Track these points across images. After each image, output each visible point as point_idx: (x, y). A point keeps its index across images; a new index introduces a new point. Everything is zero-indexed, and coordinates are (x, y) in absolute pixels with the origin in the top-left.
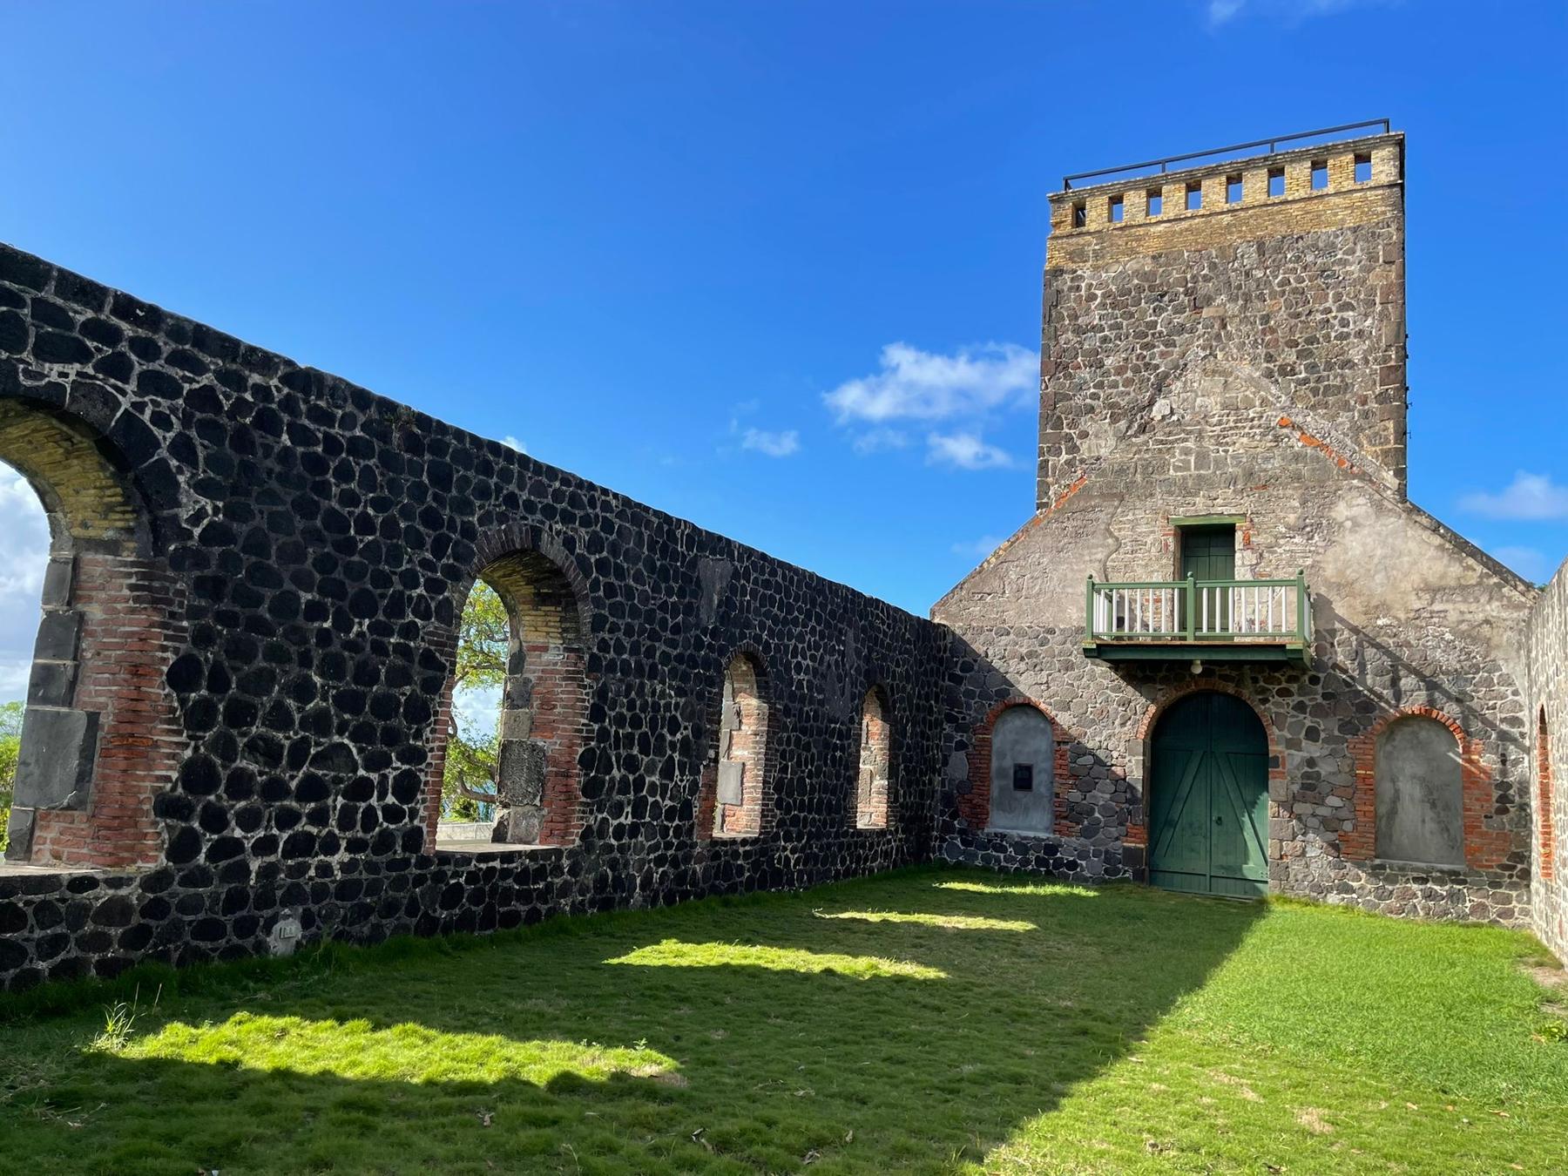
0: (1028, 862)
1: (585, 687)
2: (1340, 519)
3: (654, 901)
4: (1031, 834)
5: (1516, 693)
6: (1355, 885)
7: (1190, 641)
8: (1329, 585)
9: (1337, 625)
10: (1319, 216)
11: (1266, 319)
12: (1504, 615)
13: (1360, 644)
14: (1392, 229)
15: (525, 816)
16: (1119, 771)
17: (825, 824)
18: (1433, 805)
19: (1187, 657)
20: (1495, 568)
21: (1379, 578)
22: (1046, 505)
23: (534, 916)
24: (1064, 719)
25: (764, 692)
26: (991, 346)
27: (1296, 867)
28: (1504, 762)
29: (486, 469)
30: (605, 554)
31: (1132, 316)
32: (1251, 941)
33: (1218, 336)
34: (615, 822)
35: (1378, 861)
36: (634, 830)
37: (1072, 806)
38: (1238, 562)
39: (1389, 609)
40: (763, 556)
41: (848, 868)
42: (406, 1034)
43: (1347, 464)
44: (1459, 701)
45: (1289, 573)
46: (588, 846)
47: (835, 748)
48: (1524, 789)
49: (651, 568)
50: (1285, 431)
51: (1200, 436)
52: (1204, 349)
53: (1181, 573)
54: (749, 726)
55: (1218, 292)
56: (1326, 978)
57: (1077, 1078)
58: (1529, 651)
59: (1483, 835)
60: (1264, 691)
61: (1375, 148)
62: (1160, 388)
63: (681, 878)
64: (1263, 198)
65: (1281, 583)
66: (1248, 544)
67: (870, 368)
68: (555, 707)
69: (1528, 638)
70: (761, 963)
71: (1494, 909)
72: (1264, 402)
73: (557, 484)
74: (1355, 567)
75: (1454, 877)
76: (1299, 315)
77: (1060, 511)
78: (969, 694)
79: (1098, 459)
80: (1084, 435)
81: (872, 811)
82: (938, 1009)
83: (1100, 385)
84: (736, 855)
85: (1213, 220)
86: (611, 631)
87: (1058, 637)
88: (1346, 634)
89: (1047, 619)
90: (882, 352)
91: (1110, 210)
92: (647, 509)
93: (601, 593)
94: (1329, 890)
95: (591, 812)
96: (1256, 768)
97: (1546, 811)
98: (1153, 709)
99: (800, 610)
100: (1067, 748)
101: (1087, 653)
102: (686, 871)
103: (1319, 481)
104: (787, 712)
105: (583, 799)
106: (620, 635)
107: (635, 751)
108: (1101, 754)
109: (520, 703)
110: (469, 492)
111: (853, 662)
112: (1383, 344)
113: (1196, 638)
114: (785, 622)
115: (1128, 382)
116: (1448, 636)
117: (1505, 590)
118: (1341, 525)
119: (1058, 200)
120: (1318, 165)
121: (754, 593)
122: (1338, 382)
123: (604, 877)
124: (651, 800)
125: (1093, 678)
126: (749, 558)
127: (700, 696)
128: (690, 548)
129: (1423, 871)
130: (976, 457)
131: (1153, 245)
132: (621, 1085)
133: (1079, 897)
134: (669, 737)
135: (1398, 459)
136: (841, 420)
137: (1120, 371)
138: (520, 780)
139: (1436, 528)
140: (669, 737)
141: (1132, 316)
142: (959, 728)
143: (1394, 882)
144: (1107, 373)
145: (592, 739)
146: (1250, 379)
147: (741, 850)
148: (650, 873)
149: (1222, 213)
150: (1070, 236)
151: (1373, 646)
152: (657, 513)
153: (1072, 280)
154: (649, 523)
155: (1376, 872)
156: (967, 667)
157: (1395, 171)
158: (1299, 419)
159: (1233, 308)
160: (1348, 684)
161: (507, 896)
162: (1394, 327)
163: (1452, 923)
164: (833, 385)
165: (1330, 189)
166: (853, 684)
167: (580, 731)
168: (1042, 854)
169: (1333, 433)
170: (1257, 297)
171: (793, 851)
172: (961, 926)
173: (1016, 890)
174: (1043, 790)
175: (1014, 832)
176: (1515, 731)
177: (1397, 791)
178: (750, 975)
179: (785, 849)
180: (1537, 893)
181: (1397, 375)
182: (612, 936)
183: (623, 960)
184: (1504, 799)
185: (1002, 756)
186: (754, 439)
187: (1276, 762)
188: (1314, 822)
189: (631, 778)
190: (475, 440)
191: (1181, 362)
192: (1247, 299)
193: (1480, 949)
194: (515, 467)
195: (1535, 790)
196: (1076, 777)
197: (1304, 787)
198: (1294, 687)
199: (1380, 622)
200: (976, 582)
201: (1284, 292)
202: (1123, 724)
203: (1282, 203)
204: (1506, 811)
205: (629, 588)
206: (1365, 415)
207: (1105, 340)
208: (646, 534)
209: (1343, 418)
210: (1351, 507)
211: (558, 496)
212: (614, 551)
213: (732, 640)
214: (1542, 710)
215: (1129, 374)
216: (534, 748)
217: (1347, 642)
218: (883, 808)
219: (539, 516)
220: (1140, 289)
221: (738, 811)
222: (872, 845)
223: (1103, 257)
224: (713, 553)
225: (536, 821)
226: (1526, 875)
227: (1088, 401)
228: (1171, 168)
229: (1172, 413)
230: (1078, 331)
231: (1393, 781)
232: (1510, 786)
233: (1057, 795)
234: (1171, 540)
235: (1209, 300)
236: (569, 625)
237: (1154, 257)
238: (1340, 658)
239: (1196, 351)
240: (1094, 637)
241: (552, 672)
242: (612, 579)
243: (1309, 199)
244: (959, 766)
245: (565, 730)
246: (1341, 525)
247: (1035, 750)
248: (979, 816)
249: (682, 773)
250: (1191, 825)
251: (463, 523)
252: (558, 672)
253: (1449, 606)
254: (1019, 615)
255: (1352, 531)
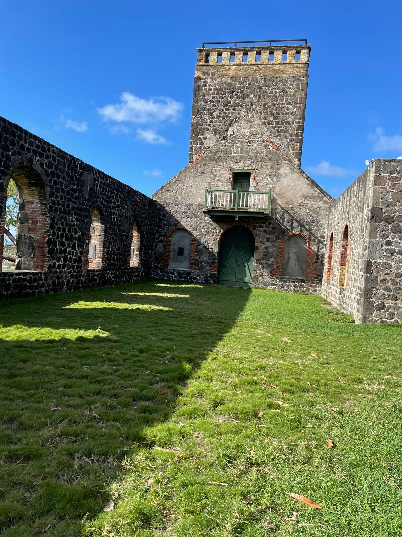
0: (181, 278)
1: (48, 217)
2: (281, 173)
3: (70, 290)
4: (183, 269)
5: (324, 229)
6: (276, 283)
7: (236, 210)
8: (277, 194)
9: (278, 207)
10: (283, 71)
11: (265, 105)
12: (323, 205)
13: (284, 213)
14: (305, 79)
15: (28, 261)
16: (210, 250)
17: (121, 265)
18: (298, 261)
19: (235, 215)
20: (322, 191)
21: (291, 192)
22: (192, 162)
23: (34, 294)
24: (195, 233)
25: (103, 221)
26: (162, 98)
27: (260, 279)
28: (318, 249)
29: (13, 134)
30: (53, 169)
31: (223, 98)
32: (251, 298)
33: (250, 109)
34: (58, 263)
35: (282, 277)
36: (64, 266)
37: (196, 261)
38: (251, 185)
39: (293, 202)
40: (103, 173)
41: (127, 279)
42: (18, 328)
43: (285, 156)
44: (308, 231)
45: (266, 190)
46: (50, 271)
47: (124, 241)
48: (323, 256)
49: (68, 175)
50: (268, 143)
51: (242, 143)
52: (245, 113)
53: (234, 188)
54: (98, 233)
55: (251, 93)
56: (274, 308)
57: (225, 333)
58: (329, 217)
59: (311, 269)
60: (255, 226)
61: (302, 49)
62: (231, 125)
63: (78, 282)
64: (267, 61)
65: (263, 193)
66: (254, 179)
67: (116, 100)
68: (37, 223)
69: (329, 213)
70: (115, 307)
71: (312, 289)
72: (262, 133)
73: (37, 142)
74: (284, 189)
75: (302, 281)
76: (275, 104)
77: (197, 164)
78: (165, 225)
79: (209, 147)
80: (205, 138)
81: (134, 262)
82: (177, 318)
83: (211, 122)
84: (94, 275)
85: (251, 67)
86: (56, 198)
87: (194, 207)
88: (280, 209)
89: (191, 201)
90: (122, 95)
91: (218, 57)
92: (67, 154)
93: (52, 184)
94: (269, 285)
95: (51, 260)
96: (251, 250)
97: (330, 262)
98: (222, 231)
99: (114, 193)
100: (195, 243)
101: (205, 212)
102: (80, 280)
103: (276, 160)
104: (110, 228)
105: (48, 255)
106: (59, 199)
107: (64, 240)
108: (205, 245)
109: (24, 221)
110: (8, 143)
111: (130, 213)
112: (298, 118)
113: (238, 209)
114: (110, 197)
115: (221, 122)
116: (308, 211)
117: (324, 198)
118: (282, 175)
119: (200, 51)
120: (285, 52)
121: (100, 186)
122: (284, 128)
123: (55, 281)
124: (69, 256)
125: (204, 221)
126: (99, 174)
127: (84, 222)
128: (80, 169)
129: (294, 279)
130: (154, 139)
131: (231, 73)
132: (97, 339)
133: (198, 288)
134: (74, 235)
135: (299, 155)
136: (105, 120)
137: (218, 117)
138: (25, 248)
139: (308, 178)
140: (74, 235)
141: (223, 98)
142: (161, 236)
143: (286, 282)
144: (214, 118)
145: (50, 235)
146: (259, 125)
147: (96, 273)
148: (69, 280)
149: (254, 65)
150: (204, 65)
151: (287, 213)
152: (70, 156)
153: (204, 82)
154: (67, 158)
155: (281, 280)
156: (164, 216)
157: (307, 58)
158: (272, 140)
159: (255, 100)
160: (279, 225)
161: (25, 287)
162: (302, 112)
163: (300, 294)
164: (102, 106)
165: (288, 62)
166: (130, 220)
167: (47, 232)
168: (186, 275)
169: (282, 145)
170: (263, 96)
171: (111, 274)
172: (168, 296)
173: (180, 286)
174: (187, 256)
175: (177, 269)
176: (322, 239)
177: (289, 257)
178: (114, 310)
179: (109, 273)
180: (324, 285)
181: (301, 128)
182: (60, 300)
183: (68, 307)
184: (317, 259)
185: (174, 245)
186: (70, 124)
187: (257, 248)
188: (266, 265)
189: (63, 249)
190: (9, 123)
191: (238, 116)
192: (260, 97)
193: (310, 300)
194: (23, 134)
195: (326, 256)
196: (197, 251)
197: (264, 255)
198: (264, 225)
199: (290, 206)
200: (167, 187)
201: (271, 96)
202: (213, 236)
203: (272, 64)
204: (318, 262)
205: (61, 182)
206: (291, 140)
207: (214, 105)
208: (67, 163)
209: (285, 141)
210: (285, 170)
211: (38, 146)
212: (56, 168)
213: (93, 203)
214: (332, 234)
215: (221, 119)
216: (30, 237)
217: (280, 212)
218: (138, 261)
219: (32, 154)
220: (226, 88)
221: (95, 262)
222: (134, 272)
223: (214, 75)
224: (88, 171)
225: (32, 263)
226: (321, 280)
227: (207, 127)
228: (239, 46)
229: (234, 134)
230: (205, 101)
231: (289, 254)
232: (319, 255)
233: (191, 257)
234: (231, 177)
235: (248, 96)
236: (42, 194)
237: (231, 78)
238: (278, 217)
239: (243, 113)
240: (207, 207)
241: (36, 211)
242: (56, 179)
243: (281, 64)
244: (160, 248)
245: (41, 232)
246: (282, 175)
247: (185, 243)
248: (166, 264)
249: (78, 248)
250: (231, 266)
251: (6, 154)
252: (38, 211)
253: (309, 202)
254: (182, 199)
255: (285, 177)
